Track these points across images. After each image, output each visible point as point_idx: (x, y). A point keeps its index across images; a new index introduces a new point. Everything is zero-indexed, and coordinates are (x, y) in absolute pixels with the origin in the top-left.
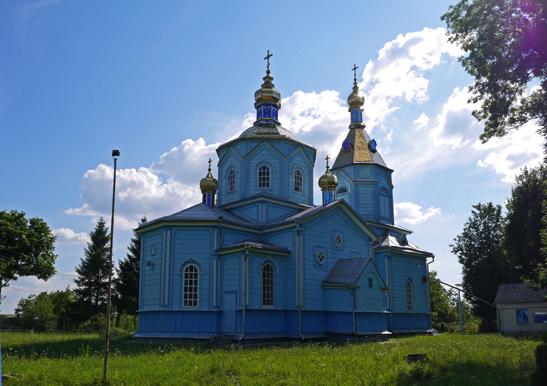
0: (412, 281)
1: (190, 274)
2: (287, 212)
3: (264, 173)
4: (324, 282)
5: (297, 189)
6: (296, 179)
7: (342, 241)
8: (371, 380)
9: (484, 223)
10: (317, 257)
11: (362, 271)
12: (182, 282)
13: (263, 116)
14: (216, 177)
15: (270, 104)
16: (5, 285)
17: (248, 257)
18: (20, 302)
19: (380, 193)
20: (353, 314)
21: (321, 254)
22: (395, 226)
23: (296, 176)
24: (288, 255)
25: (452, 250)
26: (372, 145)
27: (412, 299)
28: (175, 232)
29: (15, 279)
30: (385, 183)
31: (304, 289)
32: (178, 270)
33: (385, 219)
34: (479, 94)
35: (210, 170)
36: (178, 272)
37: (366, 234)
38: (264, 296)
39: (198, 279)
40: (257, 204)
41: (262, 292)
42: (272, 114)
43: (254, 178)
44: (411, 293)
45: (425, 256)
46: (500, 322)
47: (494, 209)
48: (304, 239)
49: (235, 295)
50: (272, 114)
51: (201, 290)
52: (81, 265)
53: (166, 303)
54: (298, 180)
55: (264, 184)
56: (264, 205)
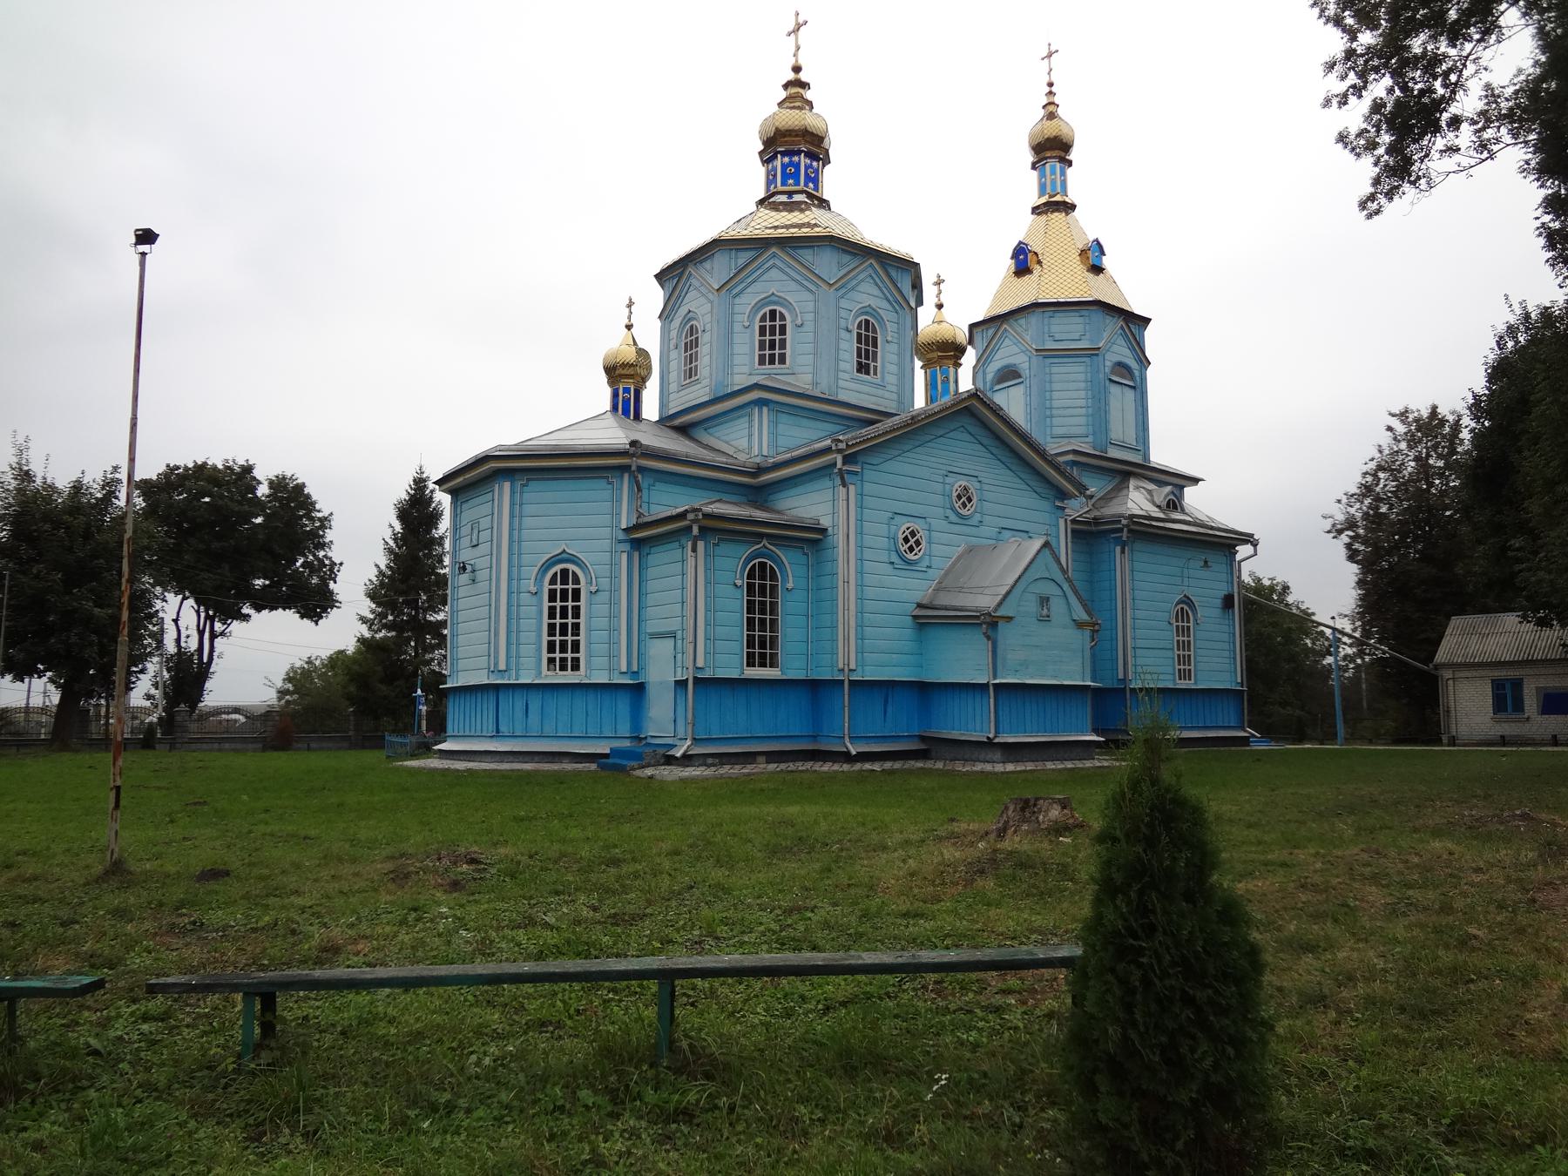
3: (773, 328)
5: (863, 368)
6: (859, 341)
8: (600, 864)
9: (1416, 459)
10: (901, 541)
11: (1017, 576)
12: (541, 612)
16: (222, 634)
18: (288, 674)
19: (1110, 380)
20: (991, 688)
21: (913, 534)
23: (859, 335)
24: (820, 537)
27: (1192, 653)
29: (246, 618)
31: (860, 626)
34: (1352, 78)
36: (532, 584)
38: (750, 644)
39: (582, 603)
41: (745, 633)
43: (746, 345)
44: (1189, 636)
45: (1235, 542)
46: (1448, 711)
47: (1443, 422)
49: (670, 642)
51: (589, 630)
52: (374, 579)
53: (502, 666)
55: (772, 357)
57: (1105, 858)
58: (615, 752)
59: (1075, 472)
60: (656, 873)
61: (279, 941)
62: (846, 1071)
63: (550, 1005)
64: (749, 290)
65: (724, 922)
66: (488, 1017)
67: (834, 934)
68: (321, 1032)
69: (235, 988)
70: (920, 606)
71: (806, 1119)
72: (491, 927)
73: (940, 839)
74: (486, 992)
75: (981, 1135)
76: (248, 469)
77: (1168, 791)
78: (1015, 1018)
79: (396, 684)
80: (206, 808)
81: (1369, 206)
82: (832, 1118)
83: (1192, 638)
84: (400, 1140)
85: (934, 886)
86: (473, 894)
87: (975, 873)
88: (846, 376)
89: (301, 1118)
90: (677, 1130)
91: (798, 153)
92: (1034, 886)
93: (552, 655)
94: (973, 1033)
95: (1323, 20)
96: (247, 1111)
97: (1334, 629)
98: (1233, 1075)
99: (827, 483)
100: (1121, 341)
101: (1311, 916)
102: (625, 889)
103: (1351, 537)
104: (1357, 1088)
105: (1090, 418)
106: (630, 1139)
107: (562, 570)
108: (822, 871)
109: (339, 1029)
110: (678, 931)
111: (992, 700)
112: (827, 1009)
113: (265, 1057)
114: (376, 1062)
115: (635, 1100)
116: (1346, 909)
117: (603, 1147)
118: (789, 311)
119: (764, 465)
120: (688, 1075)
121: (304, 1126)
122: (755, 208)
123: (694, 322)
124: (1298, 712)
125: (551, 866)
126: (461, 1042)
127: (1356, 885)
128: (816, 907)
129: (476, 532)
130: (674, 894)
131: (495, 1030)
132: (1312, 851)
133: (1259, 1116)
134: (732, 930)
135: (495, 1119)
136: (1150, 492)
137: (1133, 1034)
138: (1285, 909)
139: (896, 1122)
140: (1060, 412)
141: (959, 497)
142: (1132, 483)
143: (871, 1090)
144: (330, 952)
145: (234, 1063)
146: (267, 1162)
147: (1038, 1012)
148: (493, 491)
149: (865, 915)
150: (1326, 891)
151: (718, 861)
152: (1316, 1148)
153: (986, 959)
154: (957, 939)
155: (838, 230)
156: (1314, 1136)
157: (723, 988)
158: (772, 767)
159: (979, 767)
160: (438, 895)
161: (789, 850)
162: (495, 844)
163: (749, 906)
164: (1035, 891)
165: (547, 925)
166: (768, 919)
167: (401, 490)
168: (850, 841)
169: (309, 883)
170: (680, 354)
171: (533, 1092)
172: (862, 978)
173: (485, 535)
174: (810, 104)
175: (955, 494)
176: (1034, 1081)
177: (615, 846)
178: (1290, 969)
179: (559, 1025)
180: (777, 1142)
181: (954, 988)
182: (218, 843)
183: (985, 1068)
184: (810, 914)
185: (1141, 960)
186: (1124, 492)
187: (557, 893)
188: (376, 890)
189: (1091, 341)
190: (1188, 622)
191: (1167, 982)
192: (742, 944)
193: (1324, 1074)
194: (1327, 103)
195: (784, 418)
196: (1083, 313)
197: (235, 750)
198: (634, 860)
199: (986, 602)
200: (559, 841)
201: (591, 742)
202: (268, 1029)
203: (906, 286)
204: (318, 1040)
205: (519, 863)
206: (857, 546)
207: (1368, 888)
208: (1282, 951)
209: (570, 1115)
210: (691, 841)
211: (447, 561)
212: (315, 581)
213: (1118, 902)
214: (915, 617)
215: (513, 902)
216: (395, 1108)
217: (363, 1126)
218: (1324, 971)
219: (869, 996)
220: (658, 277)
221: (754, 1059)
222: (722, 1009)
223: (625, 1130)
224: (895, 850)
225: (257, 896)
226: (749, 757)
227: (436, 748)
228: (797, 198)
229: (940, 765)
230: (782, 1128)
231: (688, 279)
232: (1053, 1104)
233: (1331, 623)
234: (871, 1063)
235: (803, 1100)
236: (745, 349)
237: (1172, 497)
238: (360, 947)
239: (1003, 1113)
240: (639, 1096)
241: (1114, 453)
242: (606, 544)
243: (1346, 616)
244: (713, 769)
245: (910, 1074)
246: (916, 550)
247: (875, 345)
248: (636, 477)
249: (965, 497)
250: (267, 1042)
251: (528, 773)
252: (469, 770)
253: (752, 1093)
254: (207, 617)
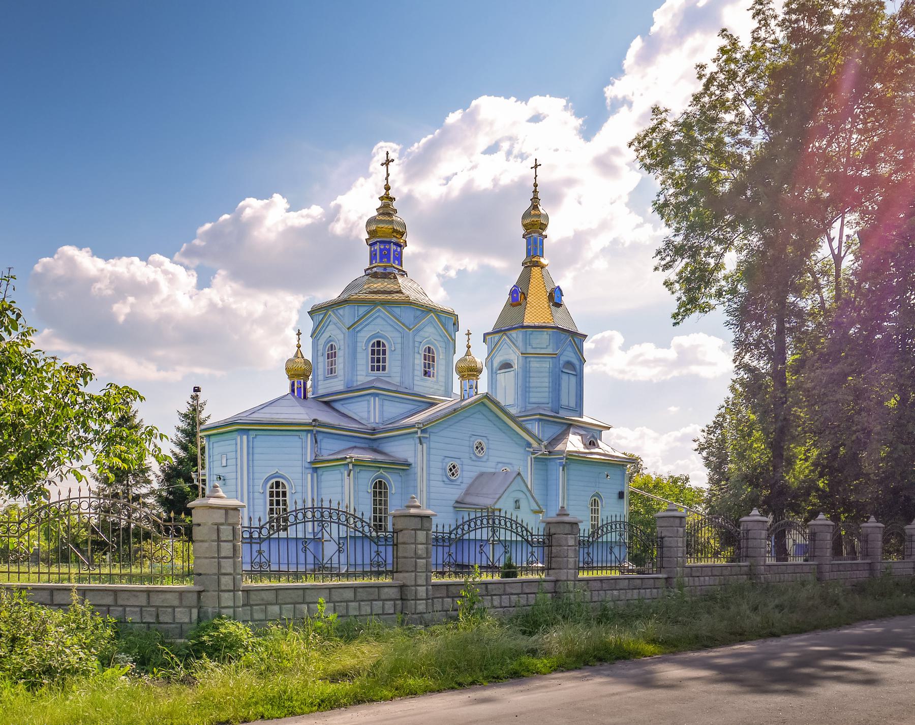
0: (599, 497)
2: (410, 407)
4: (457, 502)
5: (426, 373)
10: (448, 470)
13: (378, 260)
14: (308, 356)
15: (390, 242)
17: (352, 472)
21: (454, 467)
22: (585, 419)
26: (555, 295)
28: (253, 438)
30: (572, 355)
33: (568, 409)
35: (299, 347)
37: (524, 438)
40: (368, 398)
42: (392, 256)
43: (364, 359)
48: (429, 448)
50: (392, 256)
54: (429, 361)
56: (377, 399)
81: (677, 318)
99: (411, 441)
107: (276, 482)
142: (572, 430)
170: (324, 360)
194: (656, 269)
195: (386, 403)
214: (455, 507)
236: (364, 362)
242: (299, 469)
249: (480, 447)
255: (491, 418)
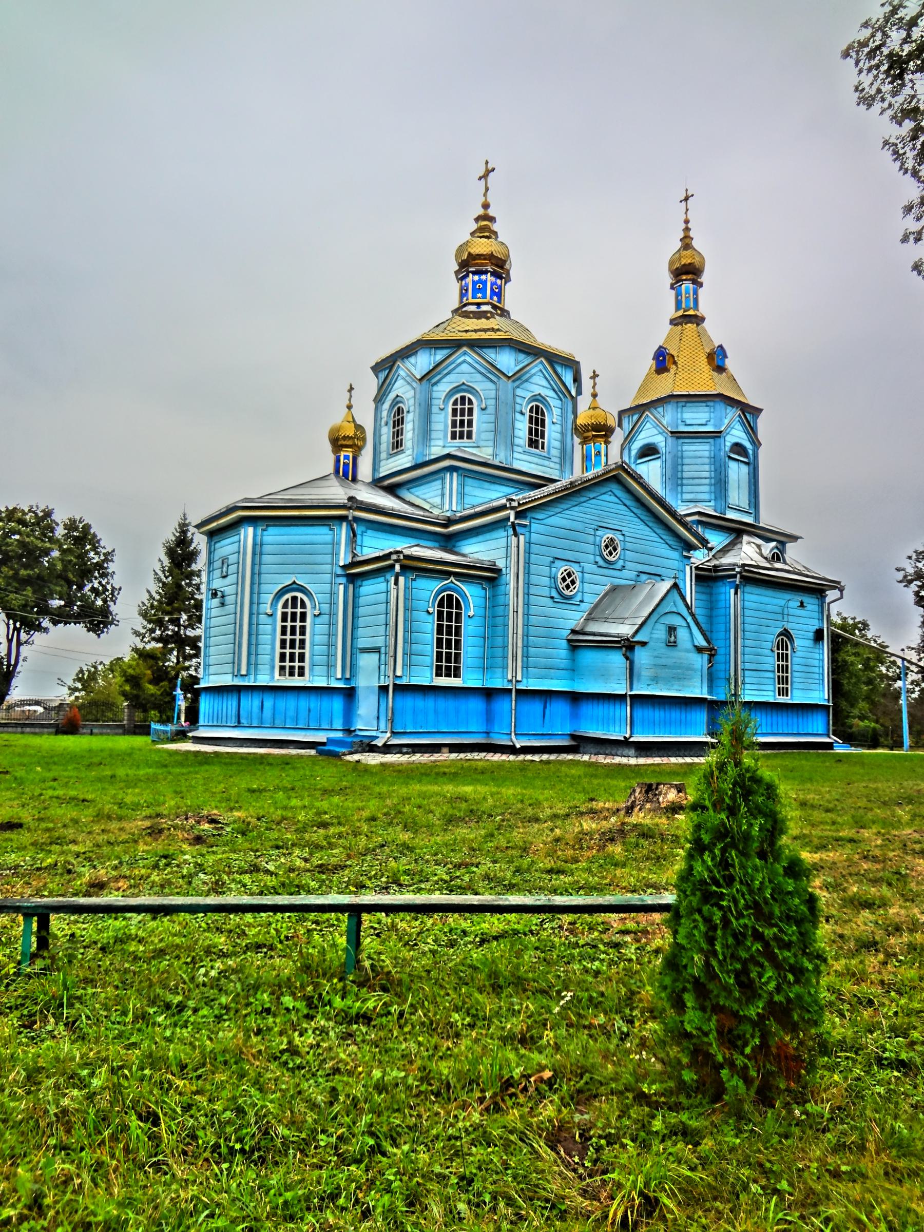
1: (292, 613)
3: (462, 411)
5: (533, 443)
6: (531, 422)
7: (619, 549)
8: (313, 826)
10: (559, 580)
11: (651, 610)
12: (274, 630)
19: (730, 458)
20: (628, 699)
21: (569, 575)
23: (531, 417)
25: (901, 578)
27: (789, 675)
29: (46, 630)
30: (743, 435)
31: (526, 646)
32: (269, 605)
43: (442, 420)
49: (376, 656)
52: (146, 602)
53: (244, 672)
57: (696, 822)
58: (330, 741)
59: (700, 530)
60: (356, 834)
61: (57, 879)
62: (494, 989)
63: (265, 933)
64: (444, 380)
65: (406, 873)
66: (216, 940)
67: (492, 885)
68: (85, 947)
69: (17, 909)
70: (574, 632)
71: (459, 1024)
72: (224, 872)
73: (582, 814)
74: (217, 920)
75: (596, 1040)
76: (48, 514)
77: (748, 770)
78: (630, 952)
79: (162, 684)
80: (8, 777)
82: (480, 1024)
83: (789, 663)
84: (139, 1030)
85: (574, 850)
86: (212, 847)
87: (607, 840)
88: (520, 450)
89: (65, 1011)
90: (357, 1030)
91: (486, 272)
92: (652, 852)
93: (283, 664)
94: (597, 963)
95: (902, 172)
96: (23, 1005)
97: (904, 659)
98: (792, 995)
99: (501, 533)
100: (738, 426)
101: (870, 880)
102: (331, 846)
103: (919, 586)
104: (896, 1013)
105: (713, 487)
106: (320, 1035)
108: (486, 836)
109: (99, 945)
110: (370, 879)
111: (629, 708)
112: (483, 942)
113: (39, 964)
114: (126, 971)
115: (326, 1005)
116: (898, 876)
117: (297, 1040)
118: (477, 399)
119: (453, 518)
120: (369, 987)
121: (67, 1018)
122: (450, 316)
123: (401, 405)
124: (873, 725)
125: (274, 827)
126: (193, 958)
127: (909, 858)
128: (479, 863)
129: (225, 565)
130: (368, 851)
131: (221, 950)
132: (874, 830)
133: (813, 1031)
134: (412, 879)
135: (216, 1017)
136: (759, 546)
137: (714, 963)
138: (850, 874)
139: (529, 1028)
140: (691, 481)
141: (607, 547)
142: (746, 538)
143: (512, 1004)
144: (98, 886)
145: (15, 967)
146: (36, 1044)
147: (648, 948)
148: (239, 534)
149: (518, 870)
150: (883, 862)
151: (405, 826)
152: (859, 1058)
153: (606, 903)
154: (589, 889)
155: (516, 335)
156: (858, 1049)
157: (403, 922)
158: (454, 756)
159: (617, 760)
160: (184, 846)
161: (462, 819)
162: (231, 809)
163: (427, 861)
164: (653, 856)
165: (267, 872)
166: (442, 873)
167: (170, 534)
168: (510, 813)
169: (83, 834)
171: (247, 997)
172: (512, 917)
173: (233, 569)
174: (495, 233)
175: (603, 544)
176: (641, 1000)
177: (326, 813)
178: (850, 920)
179: (272, 948)
180: (434, 1040)
181: (584, 928)
182: (16, 802)
183: (602, 989)
184: (475, 869)
185: (722, 903)
186: (739, 546)
187: (278, 847)
188: (136, 842)
189: (715, 426)
190: (787, 650)
191: (742, 921)
192: (421, 889)
193: (870, 1003)
195: (469, 481)
196: (709, 404)
197: (35, 734)
198: (339, 824)
199: (626, 630)
200: (282, 808)
201: (312, 732)
202: (43, 943)
203: (568, 378)
204: (82, 954)
205: (249, 823)
206: (524, 583)
207: (917, 860)
208: (845, 907)
209: (275, 1016)
210: (385, 810)
211: (203, 588)
212: (99, 602)
213: (705, 857)
214: (569, 641)
215: (242, 853)
216: (138, 1005)
217: (113, 1019)
218: (877, 923)
219: (516, 932)
220: (373, 368)
221: (421, 978)
222: (400, 939)
223: (317, 1029)
224: (546, 822)
225: (43, 844)
226: (435, 748)
227: (190, 735)
228: (484, 308)
229: (586, 758)
230: (439, 1031)
231: (397, 370)
232: (654, 1018)
233: (901, 654)
234: (513, 983)
235: (457, 1009)
237: (776, 551)
238: (120, 884)
239: (614, 1025)
240: (330, 1003)
241: (730, 515)
243: (913, 649)
244: (407, 756)
245: (543, 992)
246: (572, 588)
247: (543, 426)
248: (352, 526)
250: (41, 953)
251: (262, 756)
252: (215, 753)
253: (418, 1003)
254: (15, 628)
255: (628, 503)
